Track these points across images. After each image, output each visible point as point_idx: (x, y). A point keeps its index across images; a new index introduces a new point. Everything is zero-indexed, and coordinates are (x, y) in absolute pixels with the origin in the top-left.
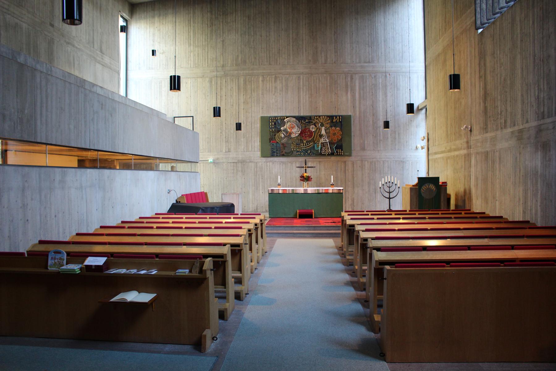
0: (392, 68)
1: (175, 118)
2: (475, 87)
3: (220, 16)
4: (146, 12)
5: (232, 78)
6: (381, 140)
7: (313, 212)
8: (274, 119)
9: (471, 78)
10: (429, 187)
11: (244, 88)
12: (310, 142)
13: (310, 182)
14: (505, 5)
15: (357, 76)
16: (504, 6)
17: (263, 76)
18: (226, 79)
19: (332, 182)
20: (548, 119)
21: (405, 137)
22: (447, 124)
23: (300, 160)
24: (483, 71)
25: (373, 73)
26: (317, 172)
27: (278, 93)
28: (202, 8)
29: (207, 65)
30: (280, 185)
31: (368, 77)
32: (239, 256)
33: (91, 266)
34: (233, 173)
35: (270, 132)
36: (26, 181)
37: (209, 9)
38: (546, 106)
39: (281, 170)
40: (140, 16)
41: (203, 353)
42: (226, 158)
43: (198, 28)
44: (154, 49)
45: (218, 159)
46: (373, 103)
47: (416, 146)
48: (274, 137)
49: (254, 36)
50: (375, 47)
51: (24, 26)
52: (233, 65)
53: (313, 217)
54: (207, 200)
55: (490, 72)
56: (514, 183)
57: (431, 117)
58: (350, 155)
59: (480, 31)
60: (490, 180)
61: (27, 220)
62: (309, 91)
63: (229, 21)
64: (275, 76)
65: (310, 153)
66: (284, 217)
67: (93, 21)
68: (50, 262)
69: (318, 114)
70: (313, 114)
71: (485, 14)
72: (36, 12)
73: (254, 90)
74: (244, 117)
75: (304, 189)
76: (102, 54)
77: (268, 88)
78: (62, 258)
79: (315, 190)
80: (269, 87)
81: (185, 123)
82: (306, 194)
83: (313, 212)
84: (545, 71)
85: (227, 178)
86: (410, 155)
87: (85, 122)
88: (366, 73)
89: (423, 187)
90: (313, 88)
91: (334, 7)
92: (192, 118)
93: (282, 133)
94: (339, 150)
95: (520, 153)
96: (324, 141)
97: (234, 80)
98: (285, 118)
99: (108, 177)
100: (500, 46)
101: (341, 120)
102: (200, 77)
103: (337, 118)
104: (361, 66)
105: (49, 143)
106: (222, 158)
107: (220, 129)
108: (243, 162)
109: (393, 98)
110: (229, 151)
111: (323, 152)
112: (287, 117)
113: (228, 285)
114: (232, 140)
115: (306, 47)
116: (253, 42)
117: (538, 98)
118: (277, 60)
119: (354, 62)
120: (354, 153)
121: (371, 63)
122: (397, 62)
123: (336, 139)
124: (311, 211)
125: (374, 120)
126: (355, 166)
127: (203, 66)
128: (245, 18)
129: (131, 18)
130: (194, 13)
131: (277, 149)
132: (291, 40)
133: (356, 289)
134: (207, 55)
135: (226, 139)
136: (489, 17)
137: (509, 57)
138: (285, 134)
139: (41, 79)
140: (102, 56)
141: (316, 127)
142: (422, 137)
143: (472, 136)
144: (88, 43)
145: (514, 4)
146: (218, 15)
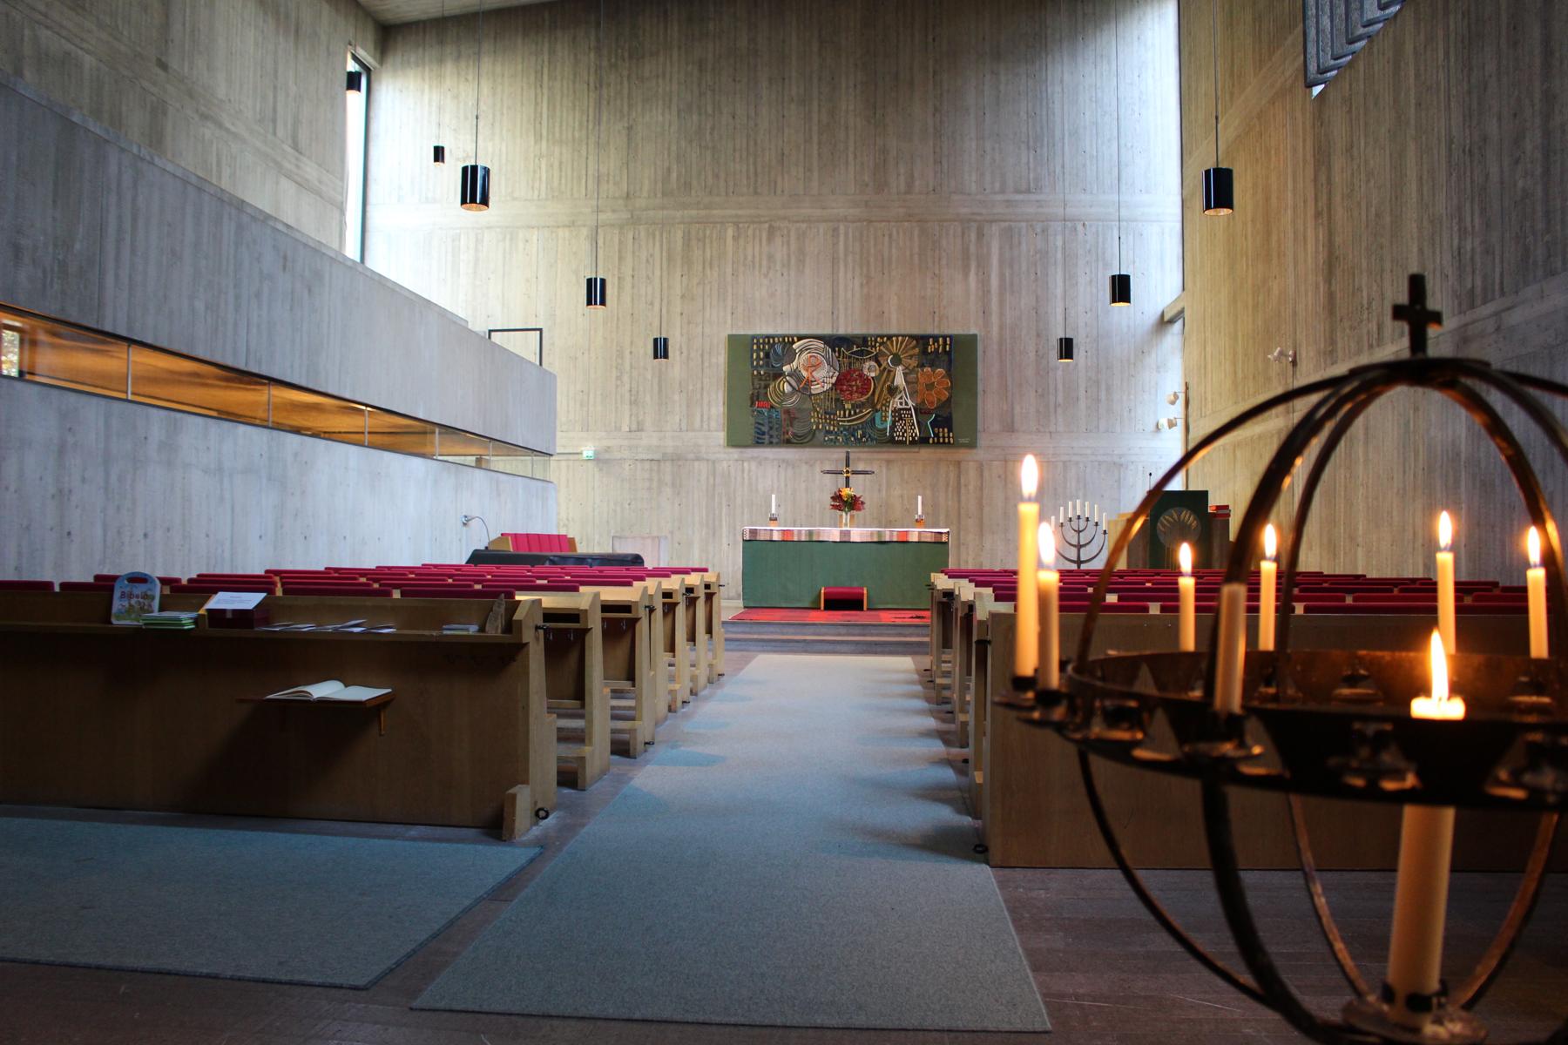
0: (1091, 207)
1: (493, 334)
2: (1305, 243)
3: (624, 60)
4: (421, 50)
5: (651, 230)
6: (1059, 405)
7: (865, 592)
8: (764, 343)
9: (1294, 222)
10: (1179, 518)
11: (683, 258)
12: (862, 406)
13: (860, 513)
14: (1379, 14)
15: (994, 228)
16: (1375, 16)
17: (736, 224)
18: (634, 233)
19: (920, 513)
20: (1483, 306)
21: (1125, 398)
22: (1235, 354)
23: (835, 456)
24: (1325, 197)
25: (1039, 221)
26: (879, 491)
27: (777, 271)
28: (574, 38)
29: (584, 194)
30: (776, 519)
31: (1024, 231)
32: (628, 640)
33: (224, 611)
34: (649, 489)
35: (753, 379)
36: (70, 429)
37: (593, 44)
38: (1478, 272)
39: (783, 485)
40: (405, 58)
41: (505, 841)
42: (630, 448)
43: (562, 92)
44: (440, 145)
45: (608, 449)
46: (1037, 301)
47: (1155, 424)
48: (764, 391)
49: (714, 117)
50: (1045, 149)
51: (88, 61)
52: (655, 195)
53: (865, 608)
54: (575, 550)
55: (1343, 199)
56: (1401, 492)
57: (1195, 339)
58: (972, 445)
59: (1317, 90)
60: (1343, 493)
61: (69, 534)
62: (861, 268)
63: (647, 74)
64: (771, 227)
65: (861, 438)
66: (784, 605)
67: (276, 62)
68: (118, 604)
69: (886, 331)
70: (872, 332)
71: (1330, 44)
72: (120, 28)
73: (711, 264)
74: (682, 335)
75: (841, 532)
76: (296, 154)
77: (750, 258)
78: (149, 593)
79: (872, 533)
80: (754, 256)
81: (524, 347)
82: (845, 543)
83: (865, 592)
84: (1476, 179)
85: (633, 503)
86: (1140, 448)
87: (237, 297)
88: (1020, 221)
89: (1162, 518)
90: (872, 260)
91: (934, 40)
92: (538, 332)
93: (787, 381)
94: (941, 430)
95: (1416, 409)
96: (901, 404)
97: (657, 233)
98: (795, 339)
99: (296, 455)
100: (1366, 124)
101: (948, 349)
102: (564, 226)
103: (938, 342)
104: (1008, 201)
105: (136, 338)
106: (621, 446)
107: (617, 368)
108: (677, 459)
109: (1094, 290)
110: (640, 429)
111: (899, 436)
112: (800, 338)
113: (592, 698)
114: (648, 398)
115: (855, 148)
116: (711, 134)
117: (1459, 253)
118: (776, 183)
119: (987, 191)
120: (983, 440)
121: (1034, 193)
122: (1104, 192)
123: (933, 399)
124: (860, 591)
125: (1041, 347)
126: (986, 474)
127: (572, 195)
128: (690, 67)
129: (382, 61)
130: (552, 52)
131: (771, 425)
132: (815, 128)
133: (947, 743)
134: (584, 166)
135: (631, 395)
136: (1339, 51)
137: (1388, 152)
138: (794, 384)
139: (120, 169)
140: (297, 159)
141: (880, 365)
142: (1170, 395)
143: (1298, 376)
144: (259, 121)
145: (1400, 10)
146: (616, 59)
